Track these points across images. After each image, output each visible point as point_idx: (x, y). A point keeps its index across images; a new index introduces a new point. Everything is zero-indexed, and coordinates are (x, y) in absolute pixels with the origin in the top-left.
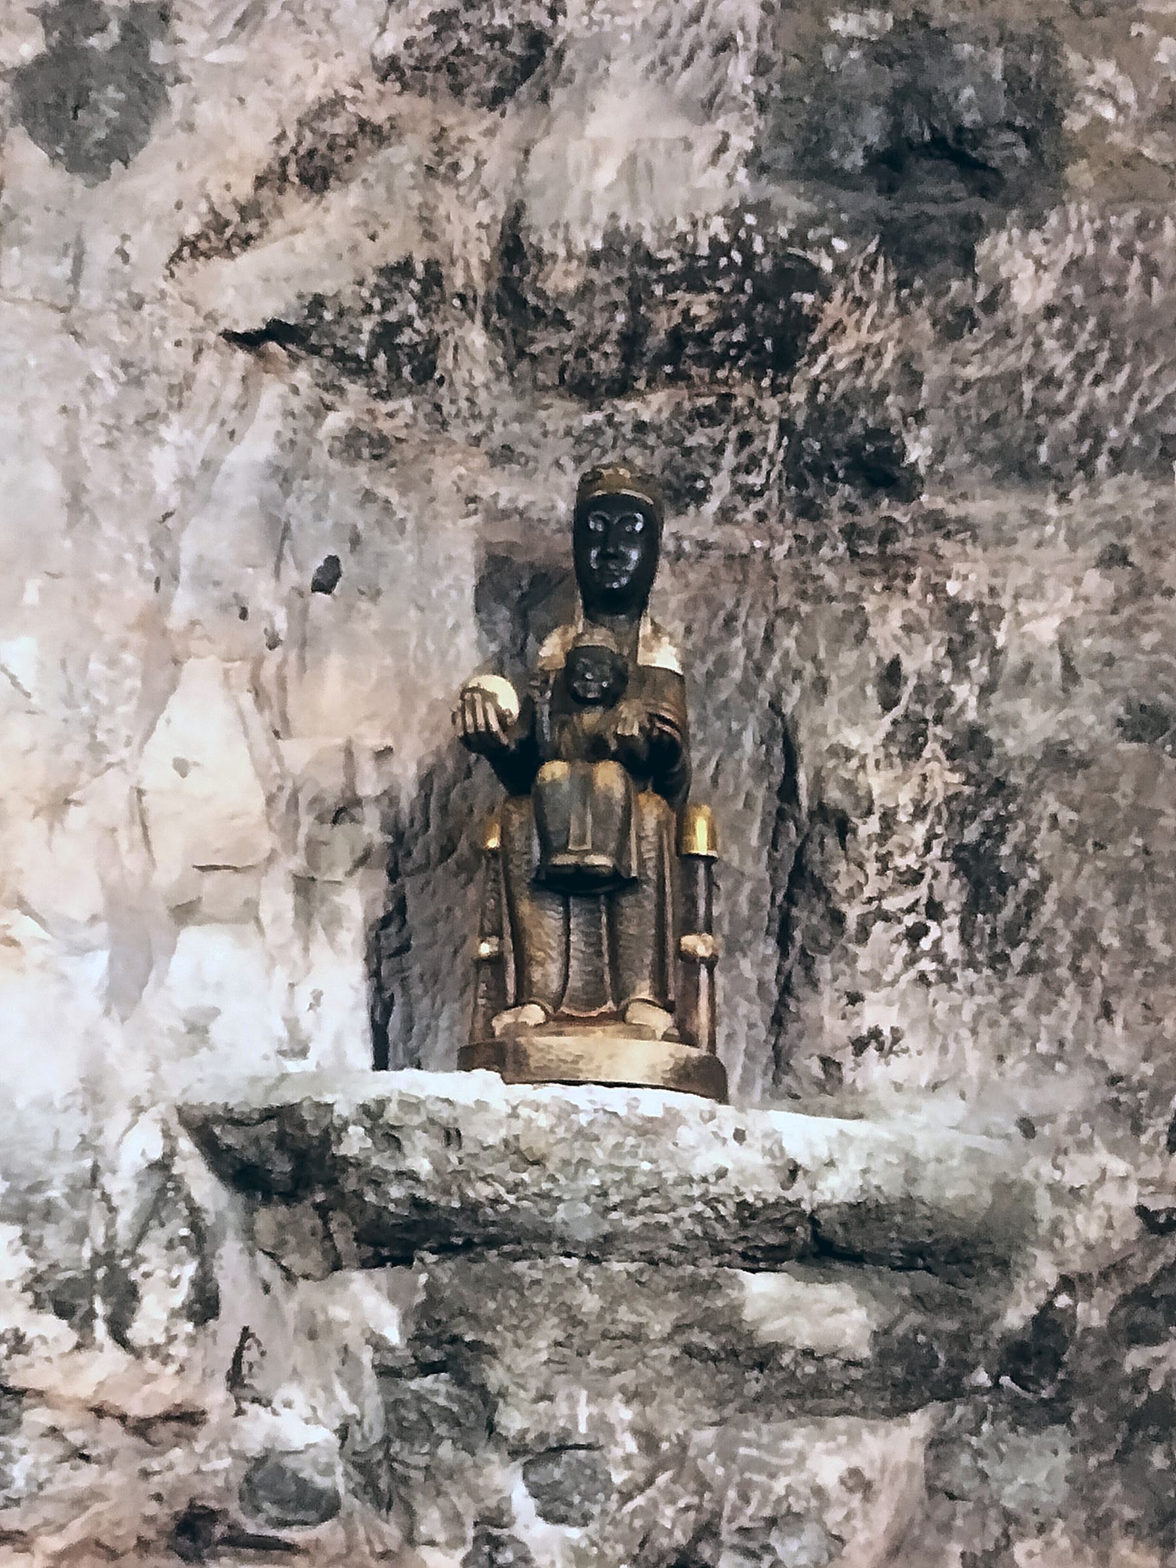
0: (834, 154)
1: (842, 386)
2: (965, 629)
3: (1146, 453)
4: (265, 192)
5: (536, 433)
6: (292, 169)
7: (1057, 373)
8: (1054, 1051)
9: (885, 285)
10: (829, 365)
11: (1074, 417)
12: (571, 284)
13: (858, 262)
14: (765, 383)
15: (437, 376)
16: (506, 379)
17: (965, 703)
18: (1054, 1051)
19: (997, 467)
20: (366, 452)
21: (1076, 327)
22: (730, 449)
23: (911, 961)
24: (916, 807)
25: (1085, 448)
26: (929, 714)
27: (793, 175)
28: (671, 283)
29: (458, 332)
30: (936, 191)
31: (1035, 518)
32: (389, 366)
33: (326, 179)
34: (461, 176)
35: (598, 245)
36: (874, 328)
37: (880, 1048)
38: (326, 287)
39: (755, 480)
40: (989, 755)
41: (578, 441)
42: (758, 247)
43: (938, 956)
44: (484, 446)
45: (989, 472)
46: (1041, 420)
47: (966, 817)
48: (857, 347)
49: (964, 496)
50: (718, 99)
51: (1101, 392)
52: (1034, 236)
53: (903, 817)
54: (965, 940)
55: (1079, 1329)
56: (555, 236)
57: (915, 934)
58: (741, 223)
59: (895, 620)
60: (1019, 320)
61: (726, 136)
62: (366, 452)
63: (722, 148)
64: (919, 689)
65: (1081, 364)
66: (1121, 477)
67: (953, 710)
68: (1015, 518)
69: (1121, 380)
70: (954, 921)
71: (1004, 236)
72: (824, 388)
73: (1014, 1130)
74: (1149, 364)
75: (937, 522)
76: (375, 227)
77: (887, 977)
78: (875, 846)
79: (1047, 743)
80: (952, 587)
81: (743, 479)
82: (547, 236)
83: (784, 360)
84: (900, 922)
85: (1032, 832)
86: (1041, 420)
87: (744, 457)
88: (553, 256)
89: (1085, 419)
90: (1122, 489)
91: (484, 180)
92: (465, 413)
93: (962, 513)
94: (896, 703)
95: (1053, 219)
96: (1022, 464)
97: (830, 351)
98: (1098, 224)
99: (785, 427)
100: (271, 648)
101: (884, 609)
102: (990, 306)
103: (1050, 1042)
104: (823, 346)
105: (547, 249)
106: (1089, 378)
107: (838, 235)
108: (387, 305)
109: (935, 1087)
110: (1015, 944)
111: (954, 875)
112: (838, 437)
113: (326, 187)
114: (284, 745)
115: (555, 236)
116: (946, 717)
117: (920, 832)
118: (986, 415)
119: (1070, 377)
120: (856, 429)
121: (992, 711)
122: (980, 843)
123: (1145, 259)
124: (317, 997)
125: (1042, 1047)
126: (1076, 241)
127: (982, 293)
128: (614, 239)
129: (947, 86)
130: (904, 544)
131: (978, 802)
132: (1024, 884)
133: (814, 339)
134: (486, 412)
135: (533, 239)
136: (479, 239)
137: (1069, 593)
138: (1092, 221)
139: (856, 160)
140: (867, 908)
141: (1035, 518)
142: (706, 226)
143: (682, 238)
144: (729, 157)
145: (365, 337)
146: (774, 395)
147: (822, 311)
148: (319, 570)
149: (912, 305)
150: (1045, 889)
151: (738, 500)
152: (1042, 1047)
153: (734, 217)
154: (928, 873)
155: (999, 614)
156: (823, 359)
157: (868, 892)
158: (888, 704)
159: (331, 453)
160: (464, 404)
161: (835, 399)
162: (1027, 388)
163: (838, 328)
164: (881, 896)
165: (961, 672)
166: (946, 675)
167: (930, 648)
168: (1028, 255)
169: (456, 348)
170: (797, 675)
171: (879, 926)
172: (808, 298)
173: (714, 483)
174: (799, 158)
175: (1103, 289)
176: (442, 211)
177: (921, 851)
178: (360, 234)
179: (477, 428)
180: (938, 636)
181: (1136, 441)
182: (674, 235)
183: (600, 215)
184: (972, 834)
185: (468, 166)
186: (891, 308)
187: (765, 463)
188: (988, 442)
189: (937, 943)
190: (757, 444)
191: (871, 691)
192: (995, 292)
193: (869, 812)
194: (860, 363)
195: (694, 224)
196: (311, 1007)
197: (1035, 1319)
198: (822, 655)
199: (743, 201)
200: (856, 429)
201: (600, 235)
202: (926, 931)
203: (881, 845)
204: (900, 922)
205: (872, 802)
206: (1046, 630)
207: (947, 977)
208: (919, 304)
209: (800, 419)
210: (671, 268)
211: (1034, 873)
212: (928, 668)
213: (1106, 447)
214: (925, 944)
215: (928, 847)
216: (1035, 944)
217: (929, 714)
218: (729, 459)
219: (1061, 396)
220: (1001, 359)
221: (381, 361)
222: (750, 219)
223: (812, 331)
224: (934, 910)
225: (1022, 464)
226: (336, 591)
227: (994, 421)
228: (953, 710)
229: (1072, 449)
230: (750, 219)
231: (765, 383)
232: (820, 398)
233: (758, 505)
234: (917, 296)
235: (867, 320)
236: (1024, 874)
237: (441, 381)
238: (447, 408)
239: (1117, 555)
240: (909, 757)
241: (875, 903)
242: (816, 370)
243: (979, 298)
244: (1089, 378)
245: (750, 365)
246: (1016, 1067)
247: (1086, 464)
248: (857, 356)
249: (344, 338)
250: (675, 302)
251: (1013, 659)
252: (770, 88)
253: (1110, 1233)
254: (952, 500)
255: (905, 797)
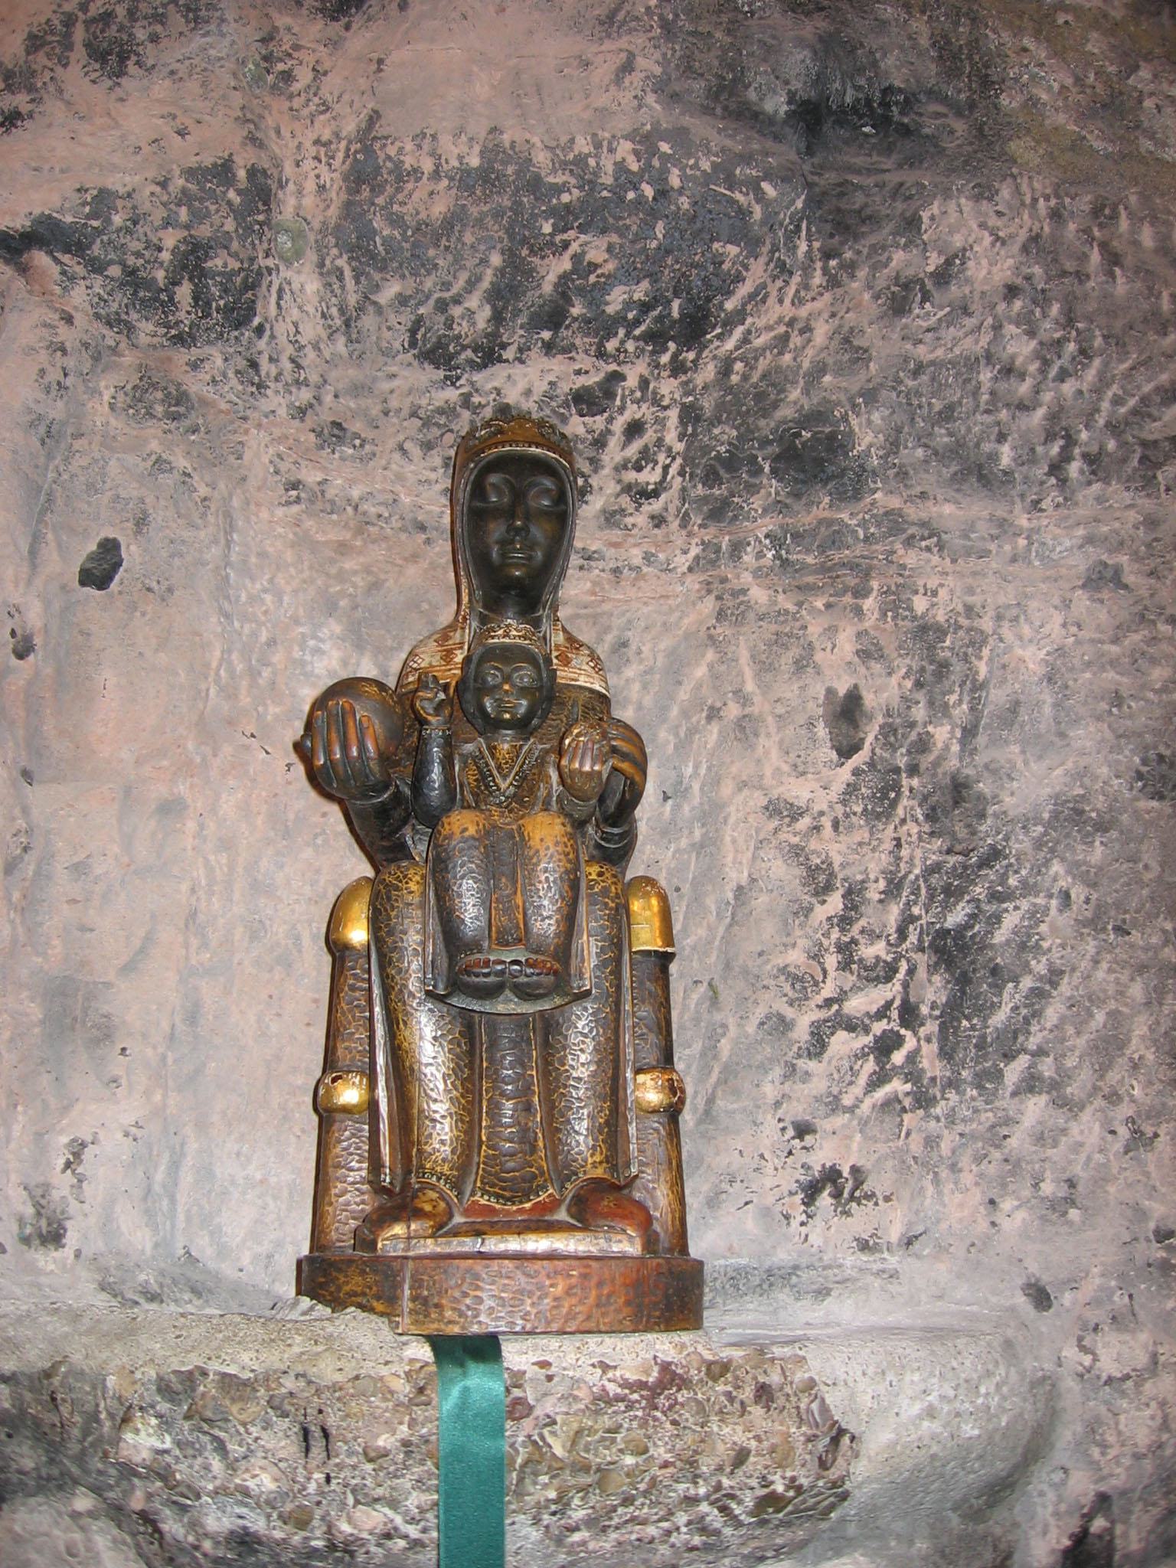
0: (752, 95)
1: (763, 364)
2: (938, 656)
3: (1124, 460)
4: (41, 59)
5: (375, 411)
6: (79, 34)
7: (1019, 361)
8: (1063, 1191)
9: (809, 253)
10: (745, 340)
11: (1040, 412)
12: (439, 209)
13: (785, 217)
14: (665, 359)
15: (256, 321)
16: (341, 340)
17: (947, 748)
18: (1063, 1191)
19: (954, 468)
20: (159, 409)
21: (1038, 311)
22: (613, 443)
23: (878, 1080)
24: (890, 882)
25: (1055, 449)
26: (902, 762)
27: (707, 111)
28: (565, 217)
29: (285, 273)
30: (859, 161)
31: (1003, 527)
32: (196, 298)
33: (123, 59)
34: (296, 87)
35: (475, 162)
36: (798, 301)
37: (837, 1195)
38: (117, 183)
39: (649, 477)
40: (982, 816)
41: (427, 423)
42: (675, 181)
43: (912, 1073)
44: (310, 420)
45: (947, 473)
46: (1004, 415)
47: (953, 893)
48: (780, 321)
49: (923, 495)
50: (620, 16)
51: (1068, 388)
52: (985, 205)
53: (873, 894)
54: (946, 1053)
55: (1117, 1557)
56: (419, 147)
57: (885, 1046)
58: (654, 151)
59: (846, 643)
60: (977, 296)
61: (631, 56)
62: (159, 409)
63: (628, 67)
64: (888, 731)
65: (1043, 359)
66: (1096, 487)
67: (931, 758)
68: (983, 528)
69: (1091, 375)
70: (931, 1027)
71: (952, 206)
72: (739, 366)
73: (1021, 1300)
74: (1121, 361)
75: (894, 523)
76: (183, 120)
77: (847, 1101)
78: (835, 934)
79: (1057, 799)
80: (920, 604)
81: (631, 476)
82: (409, 146)
83: (694, 329)
84: (867, 1030)
85: (1036, 916)
86: (1004, 415)
87: (633, 450)
88: (416, 172)
89: (1053, 417)
90: (1099, 500)
91: (325, 92)
92: (288, 377)
93: (924, 515)
94: (856, 748)
95: (1005, 192)
96: (980, 467)
97: (749, 320)
98: (1053, 202)
99: (690, 415)
100: (21, 655)
101: (832, 630)
102: (942, 277)
103: (1056, 1181)
104: (740, 316)
105: (409, 162)
106: (1053, 372)
107: (767, 176)
108: (198, 216)
109: (909, 1243)
110: (1009, 1057)
111: (932, 969)
112: (762, 423)
113: (121, 73)
114: (35, 795)
115: (419, 147)
116: (923, 767)
117: (894, 913)
118: (938, 405)
119: (1033, 367)
120: (785, 412)
121: (980, 759)
122: (967, 926)
123: (1104, 246)
124: (77, 1150)
125: (1047, 1188)
126: (1031, 216)
127: (934, 261)
128: (493, 153)
129: (872, 42)
130: (853, 552)
131: (967, 874)
132: (1027, 982)
133: (729, 305)
134: (314, 378)
135: (392, 151)
136: (317, 159)
137: (1058, 618)
138: (1047, 198)
139: (777, 104)
140: (823, 1014)
141: (1003, 527)
142: (611, 150)
143: (581, 160)
144: (635, 79)
145: (165, 256)
146: (674, 374)
147: (747, 268)
148: (91, 558)
149: (844, 277)
150: (1054, 985)
151: (625, 501)
152: (1047, 1188)
153: (645, 142)
154: (904, 966)
155: (978, 640)
156: (738, 332)
157: (828, 990)
158: (846, 751)
159: (112, 407)
160: (288, 366)
161: (755, 378)
162: (986, 376)
163: (758, 297)
164: (840, 998)
165: (939, 710)
166: (919, 713)
167: (894, 680)
168: (982, 226)
169: (280, 291)
170: (713, 714)
171: (842, 1035)
172: (733, 250)
173: (594, 481)
174: (714, 94)
175: (1064, 273)
176: (270, 121)
177: (893, 938)
178: (167, 129)
179: (305, 395)
180: (902, 665)
181: (1111, 445)
182: (571, 156)
183: (479, 128)
184: (956, 917)
185: (304, 77)
186: (818, 279)
187: (662, 458)
188: (942, 438)
189: (912, 1057)
190: (649, 436)
191: (822, 731)
192: (949, 262)
193: (829, 888)
194: (785, 339)
195: (598, 145)
196: (68, 1165)
197: (1067, 1553)
198: (750, 687)
199: (656, 125)
200: (785, 412)
201: (477, 149)
202: (898, 1041)
203: (843, 930)
204: (867, 1030)
205: (832, 875)
206: (1032, 658)
207: (923, 1100)
208: (853, 276)
209: (708, 404)
210: (565, 198)
211: (1040, 967)
212: (895, 703)
213: (1077, 451)
214: (898, 1057)
215: (902, 934)
216: (1040, 1052)
217: (902, 762)
218: (614, 452)
219: (1024, 388)
220: (956, 341)
221: (184, 292)
222: (665, 147)
223: (729, 293)
224: (909, 1015)
225: (980, 467)
226: (114, 586)
227: (947, 414)
228: (931, 758)
229: (1040, 449)
230: (665, 147)
231: (665, 359)
232: (735, 379)
233: (655, 506)
234: (850, 268)
235: (791, 291)
236: (1027, 969)
237: (260, 331)
238: (265, 366)
239: (1109, 574)
240: (878, 816)
241: (836, 1007)
242: (730, 344)
243: (931, 269)
244: (1053, 372)
245: (649, 337)
246: (1015, 1217)
247: (1056, 468)
248: (782, 329)
249: (138, 255)
250: (566, 245)
251: (997, 696)
252: (677, 16)
253: (1165, 1437)
254: (909, 499)
255: (876, 864)
